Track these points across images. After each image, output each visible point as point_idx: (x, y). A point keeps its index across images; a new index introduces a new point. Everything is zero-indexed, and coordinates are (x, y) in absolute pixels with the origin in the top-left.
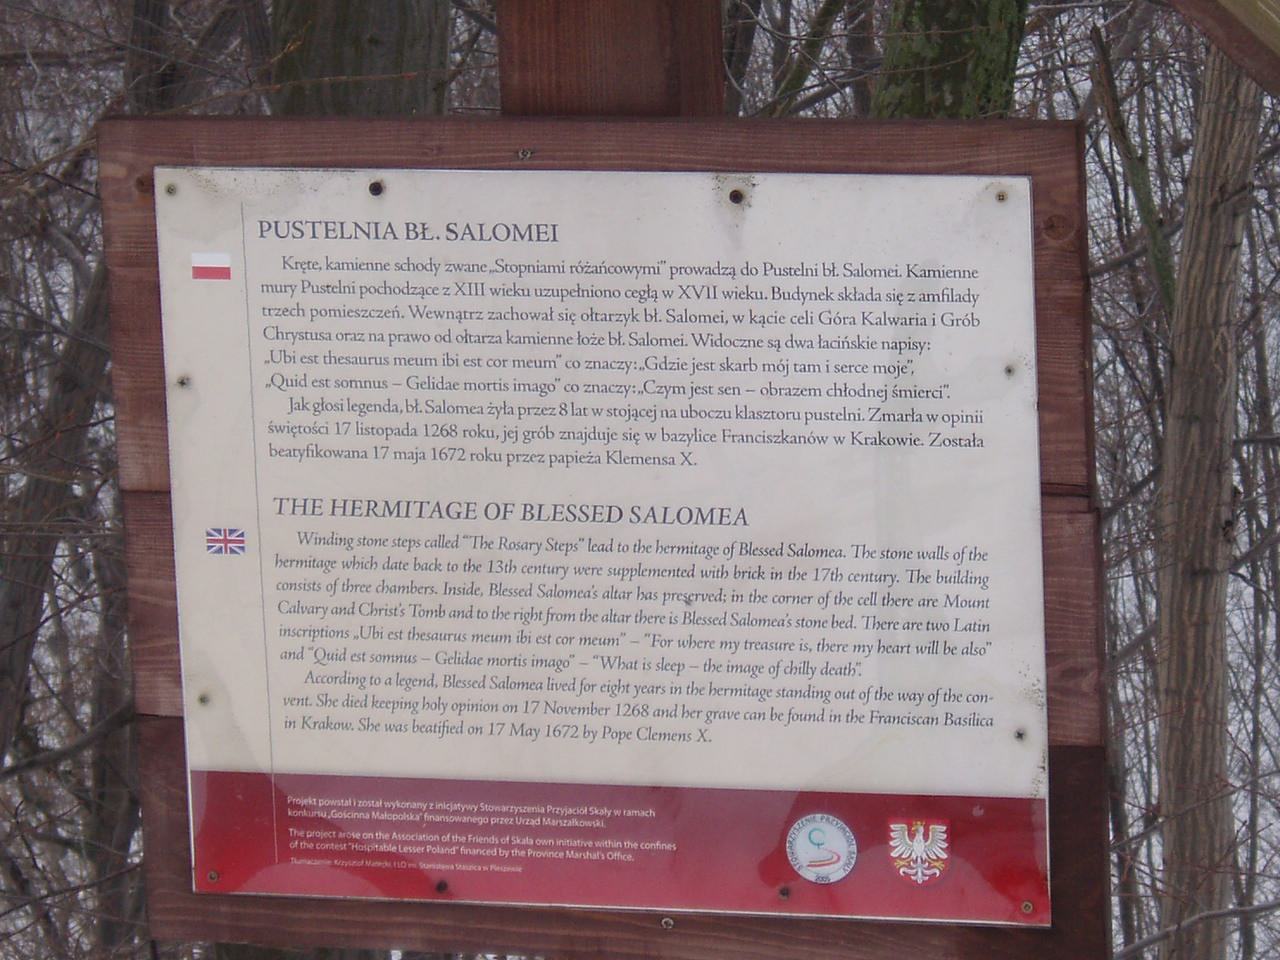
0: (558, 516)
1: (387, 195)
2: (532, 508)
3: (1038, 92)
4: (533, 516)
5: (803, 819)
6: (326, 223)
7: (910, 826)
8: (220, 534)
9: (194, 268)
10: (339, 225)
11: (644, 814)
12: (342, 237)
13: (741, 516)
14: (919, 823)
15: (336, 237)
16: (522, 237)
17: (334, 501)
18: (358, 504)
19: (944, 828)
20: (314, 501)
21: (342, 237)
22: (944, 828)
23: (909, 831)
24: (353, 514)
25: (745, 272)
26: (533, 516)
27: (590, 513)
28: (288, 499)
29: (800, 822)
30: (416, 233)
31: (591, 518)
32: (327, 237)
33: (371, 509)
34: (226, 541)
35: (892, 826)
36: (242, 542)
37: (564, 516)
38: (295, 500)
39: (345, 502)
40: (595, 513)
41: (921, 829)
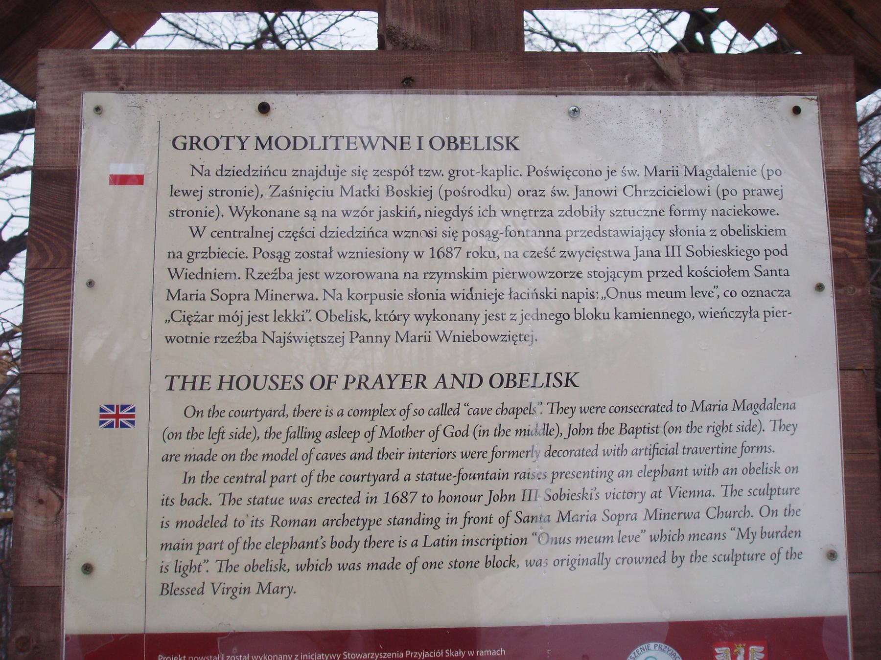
0: (287, 386)
1: (274, 113)
2: (515, 376)
3: (300, 31)
4: (515, 384)
5: (639, 648)
6: (348, 138)
7: (732, 649)
8: (114, 411)
9: (110, 175)
10: (473, 140)
11: (495, 653)
12: (476, 149)
13: (379, 381)
14: (740, 645)
15: (470, 149)
16: (263, 147)
17: (222, 377)
18: (408, 378)
19: (762, 649)
20: (203, 377)
21: (476, 149)
22: (762, 649)
23: (732, 651)
24: (201, 389)
25: (219, 173)
26: (515, 384)
27: (280, 382)
28: (179, 376)
29: (635, 651)
30: (456, 144)
31: (280, 387)
32: (348, 148)
33: (252, 382)
34: (117, 416)
35: (717, 650)
36: (102, 416)
37: (291, 385)
38: (185, 377)
39: (195, 377)
40: (284, 382)
41: (743, 651)
